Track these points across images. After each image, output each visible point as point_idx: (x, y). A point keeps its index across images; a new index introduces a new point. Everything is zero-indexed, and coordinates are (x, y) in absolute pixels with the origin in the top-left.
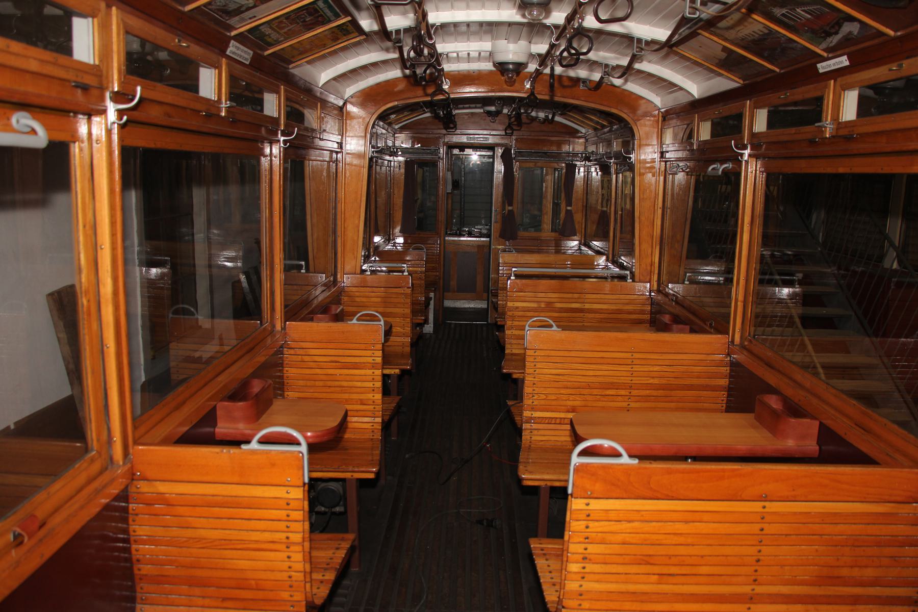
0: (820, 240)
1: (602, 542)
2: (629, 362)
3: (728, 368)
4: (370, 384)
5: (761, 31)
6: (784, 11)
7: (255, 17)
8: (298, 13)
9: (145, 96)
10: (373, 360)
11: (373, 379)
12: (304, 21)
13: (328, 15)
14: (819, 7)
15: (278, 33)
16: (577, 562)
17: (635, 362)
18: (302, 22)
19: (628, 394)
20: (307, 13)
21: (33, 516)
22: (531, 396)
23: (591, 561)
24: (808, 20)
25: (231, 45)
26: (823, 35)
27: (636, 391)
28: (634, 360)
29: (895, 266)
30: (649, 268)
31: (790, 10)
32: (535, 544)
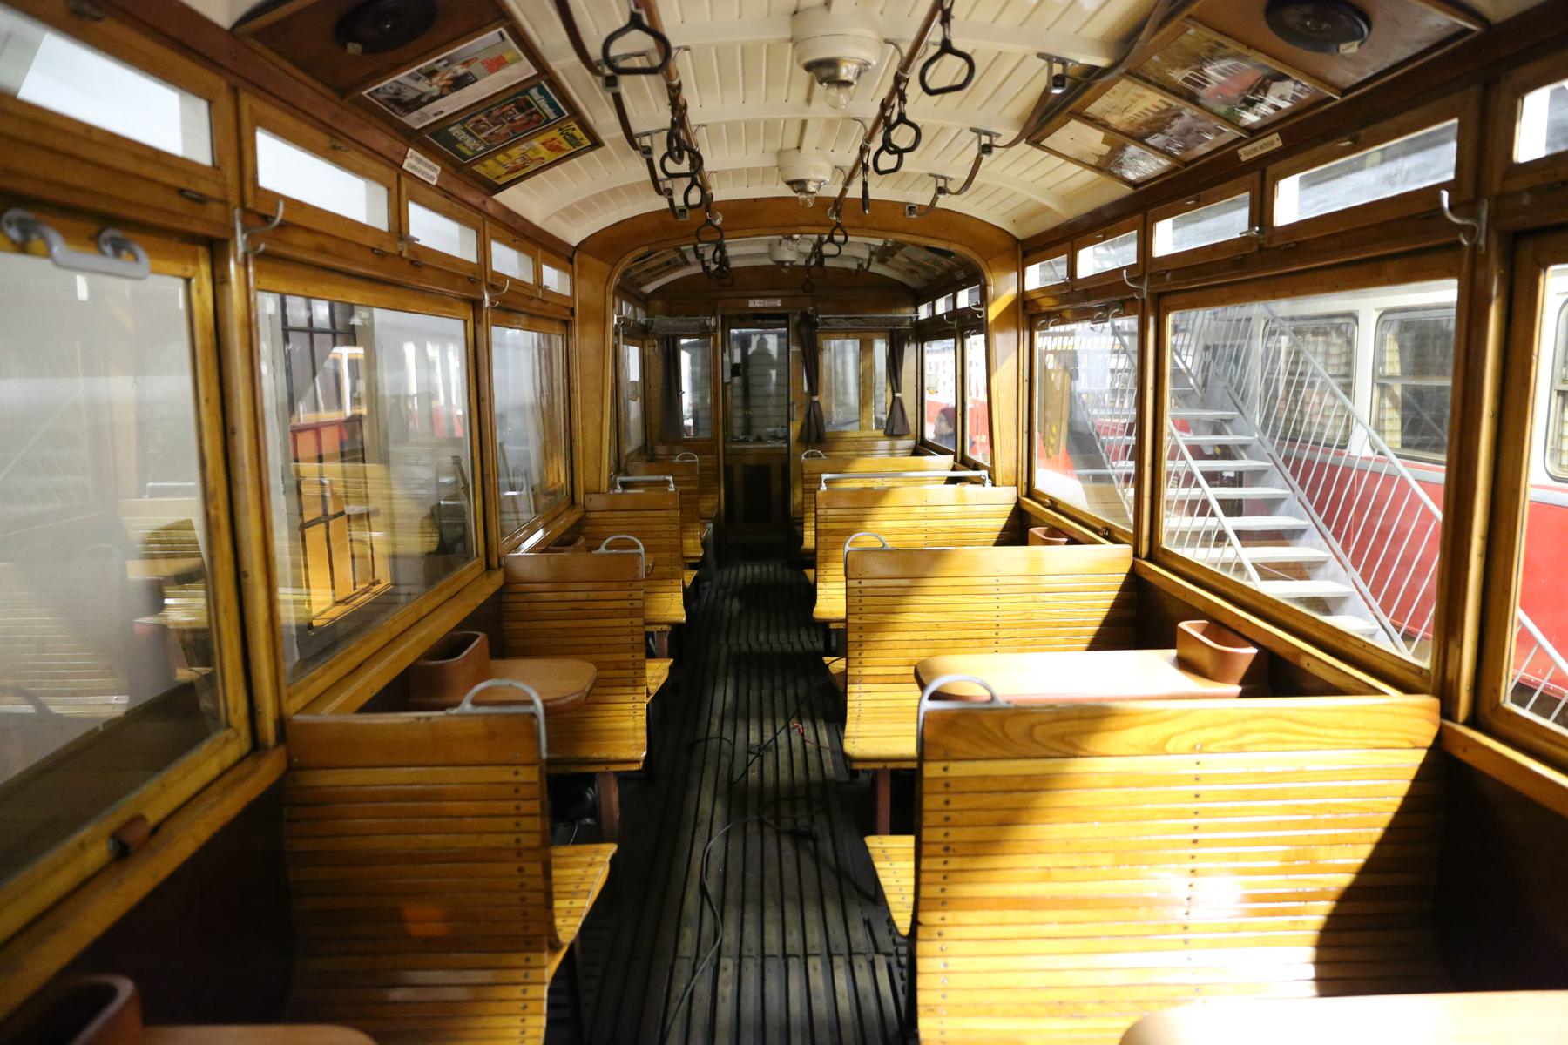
4: (628, 639)
5: (1157, 107)
6: (1187, 73)
7: (441, 112)
8: (503, 107)
9: (288, 219)
11: (632, 631)
12: (512, 121)
13: (546, 111)
17: (1002, 590)
18: (509, 122)
20: (517, 108)
21: (138, 819)
25: (409, 155)
26: (1244, 105)
28: (999, 578)
31: (1196, 71)
32: (872, 842)
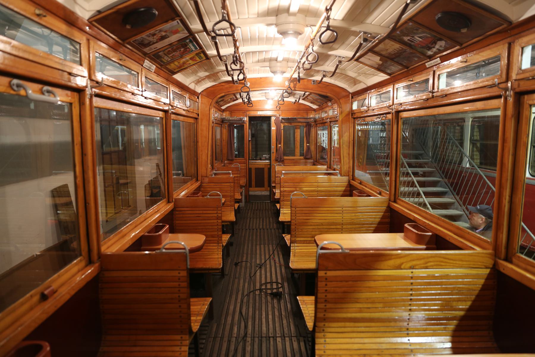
0: (430, 155)
1: (334, 292)
2: (341, 212)
3: (389, 213)
5: (398, 49)
6: (409, 38)
10: (217, 215)
14: (425, 34)
15: (168, 56)
16: (322, 303)
17: (344, 212)
19: (341, 227)
22: (294, 230)
23: (329, 302)
24: (420, 41)
27: (345, 226)
29: (468, 166)
30: (348, 169)
31: (412, 37)
